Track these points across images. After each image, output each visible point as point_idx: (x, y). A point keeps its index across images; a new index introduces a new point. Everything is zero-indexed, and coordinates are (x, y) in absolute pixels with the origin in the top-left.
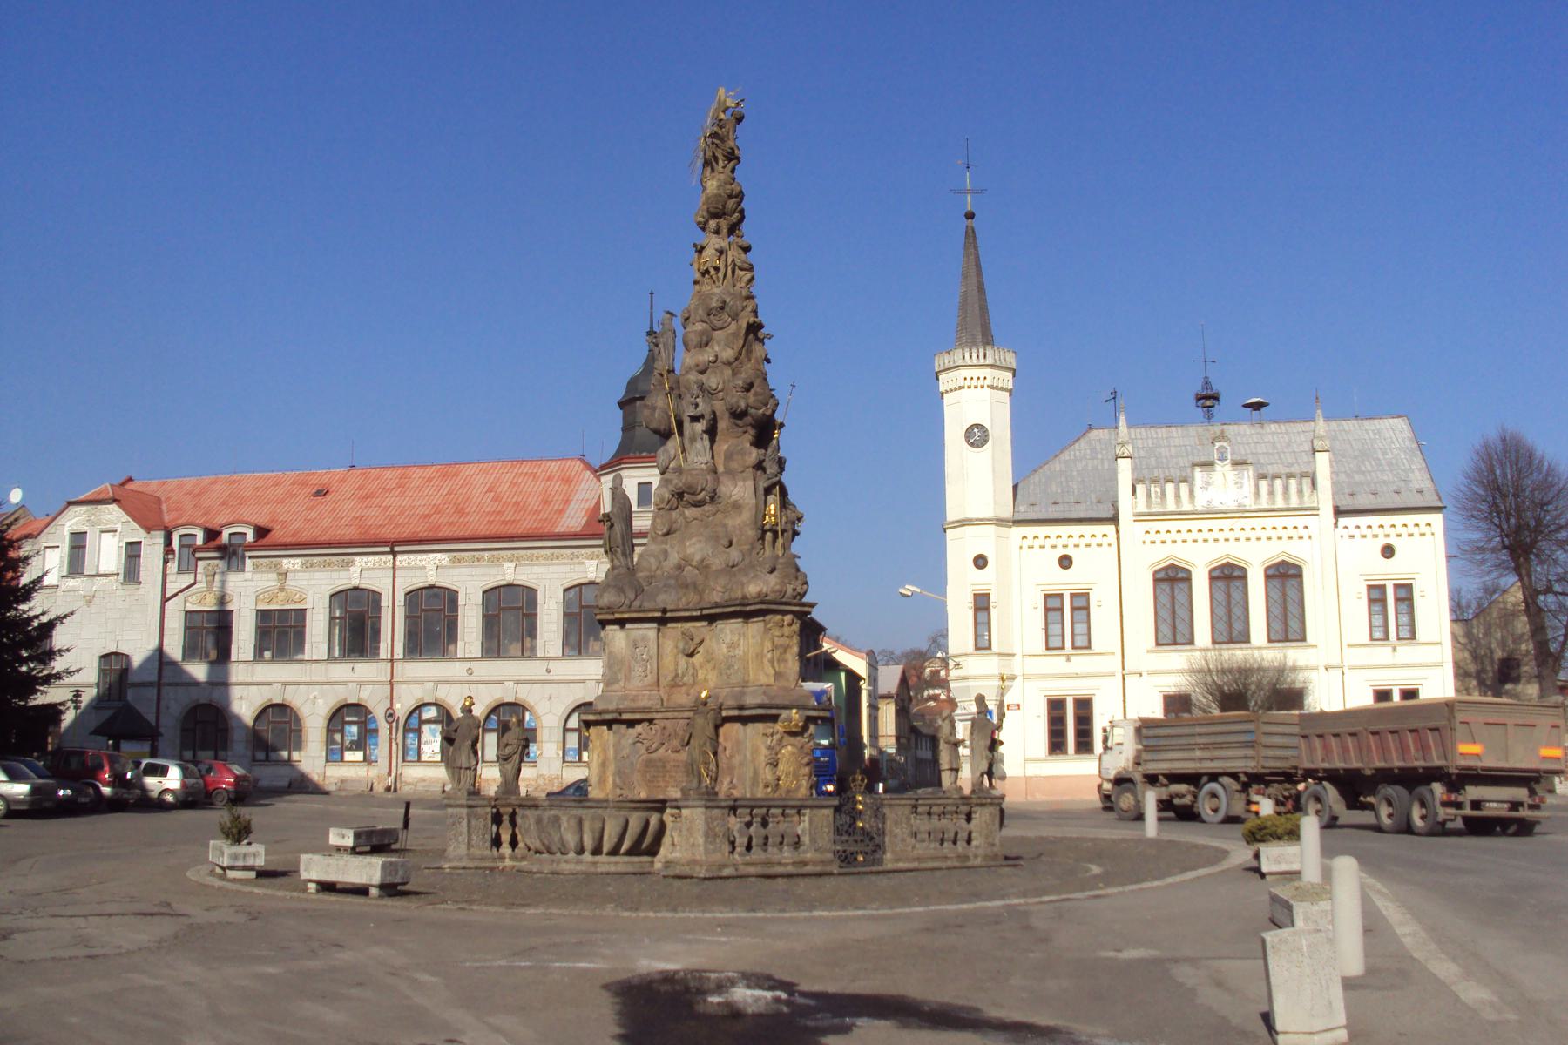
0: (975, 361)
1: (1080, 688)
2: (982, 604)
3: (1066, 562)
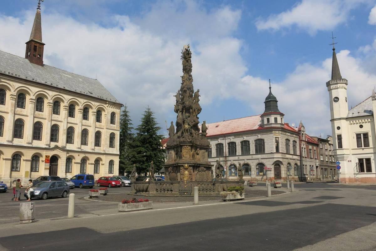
1: (367, 156)
2: (112, 122)
3: (361, 126)
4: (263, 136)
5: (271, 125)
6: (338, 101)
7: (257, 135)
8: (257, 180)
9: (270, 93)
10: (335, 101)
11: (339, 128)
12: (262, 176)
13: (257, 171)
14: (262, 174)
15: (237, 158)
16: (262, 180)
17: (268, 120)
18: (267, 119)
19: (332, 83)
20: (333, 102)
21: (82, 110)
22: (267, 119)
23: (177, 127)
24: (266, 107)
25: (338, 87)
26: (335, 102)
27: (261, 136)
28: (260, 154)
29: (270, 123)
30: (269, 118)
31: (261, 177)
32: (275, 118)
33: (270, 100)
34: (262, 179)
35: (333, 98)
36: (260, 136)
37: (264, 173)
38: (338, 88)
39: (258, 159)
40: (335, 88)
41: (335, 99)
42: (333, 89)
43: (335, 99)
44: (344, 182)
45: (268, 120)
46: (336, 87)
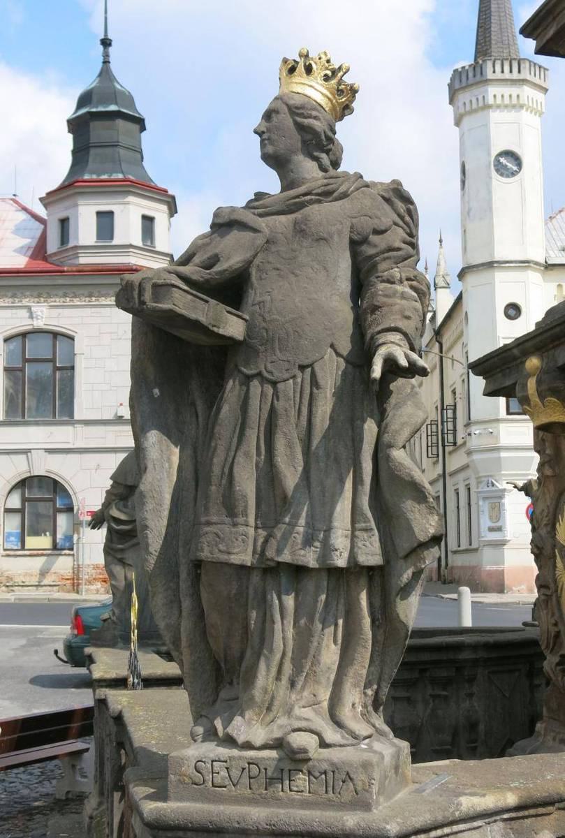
0: (507, 75)
4: (66, 312)
5: (127, 254)
6: (513, 174)
7: (25, 302)
8: (9, 578)
9: (105, 72)
10: (501, 170)
11: (512, 312)
12: (43, 559)
13: (14, 524)
14: (44, 542)
15: (328, 661)
16: (45, 582)
17: (106, 221)
18: (100, 214)
19: (498, 75)
20: (494, 173)
21: (119, 420)
22: (100, 214)
23: (131, 595)
24: (81, 153)
25: (523, 100)
26: (502, 175)
27: (56, 312)
28: (37, 423)
29: (115, 242)
30: (110, 214)
31: (39, 562)
32: (99, 213)
33: (113, 108)
34: (43, 573)
35: (494, 153)
36: (46, 314)
37: (59, 536)
38: (522, 107)
39: (26, 452)
40: (507, 101)
41: (502, 160)
42: (498, 107)
43: (502, 160)
44: (523, 587)
45: (106, 221)
46: (514, 101)
